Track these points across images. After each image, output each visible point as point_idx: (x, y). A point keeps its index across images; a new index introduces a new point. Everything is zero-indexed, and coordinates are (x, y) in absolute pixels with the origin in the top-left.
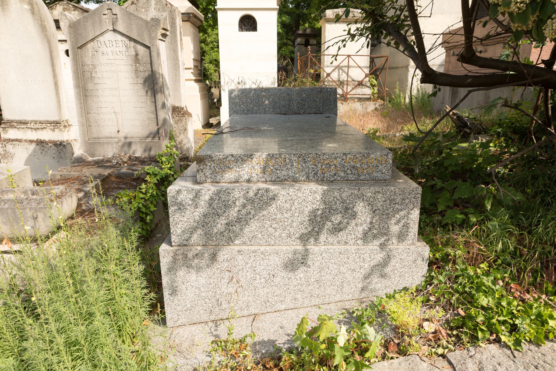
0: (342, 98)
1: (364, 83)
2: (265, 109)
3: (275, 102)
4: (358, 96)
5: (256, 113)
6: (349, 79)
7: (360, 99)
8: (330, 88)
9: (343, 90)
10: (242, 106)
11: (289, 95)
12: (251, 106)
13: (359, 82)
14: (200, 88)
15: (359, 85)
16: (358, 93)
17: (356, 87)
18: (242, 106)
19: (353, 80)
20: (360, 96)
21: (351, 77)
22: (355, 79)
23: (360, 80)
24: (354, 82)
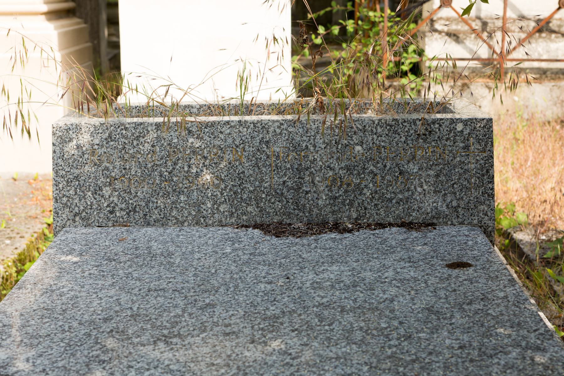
0: (488, 71)
1: (553, 25)
2: (198, 205)
3: (241, 177)
4: (536, 64)
5: (163, 222)
6: (510, 14)
7: (543, 75)
8: (466, 122)
9: (490, 47)
10: (107, 191)
11: (296, 147)
12: (143, 191)
13: (538, 21)
14: (63, 36)
15: (540, 31)
16: (535, 56)
17: (530, 35)
18: (107, 191)
19: (522, 18)
20: (544, 65)
21: (514, 8)
22: (526, 13)
23: (545, 15)
24: (523, 23)
